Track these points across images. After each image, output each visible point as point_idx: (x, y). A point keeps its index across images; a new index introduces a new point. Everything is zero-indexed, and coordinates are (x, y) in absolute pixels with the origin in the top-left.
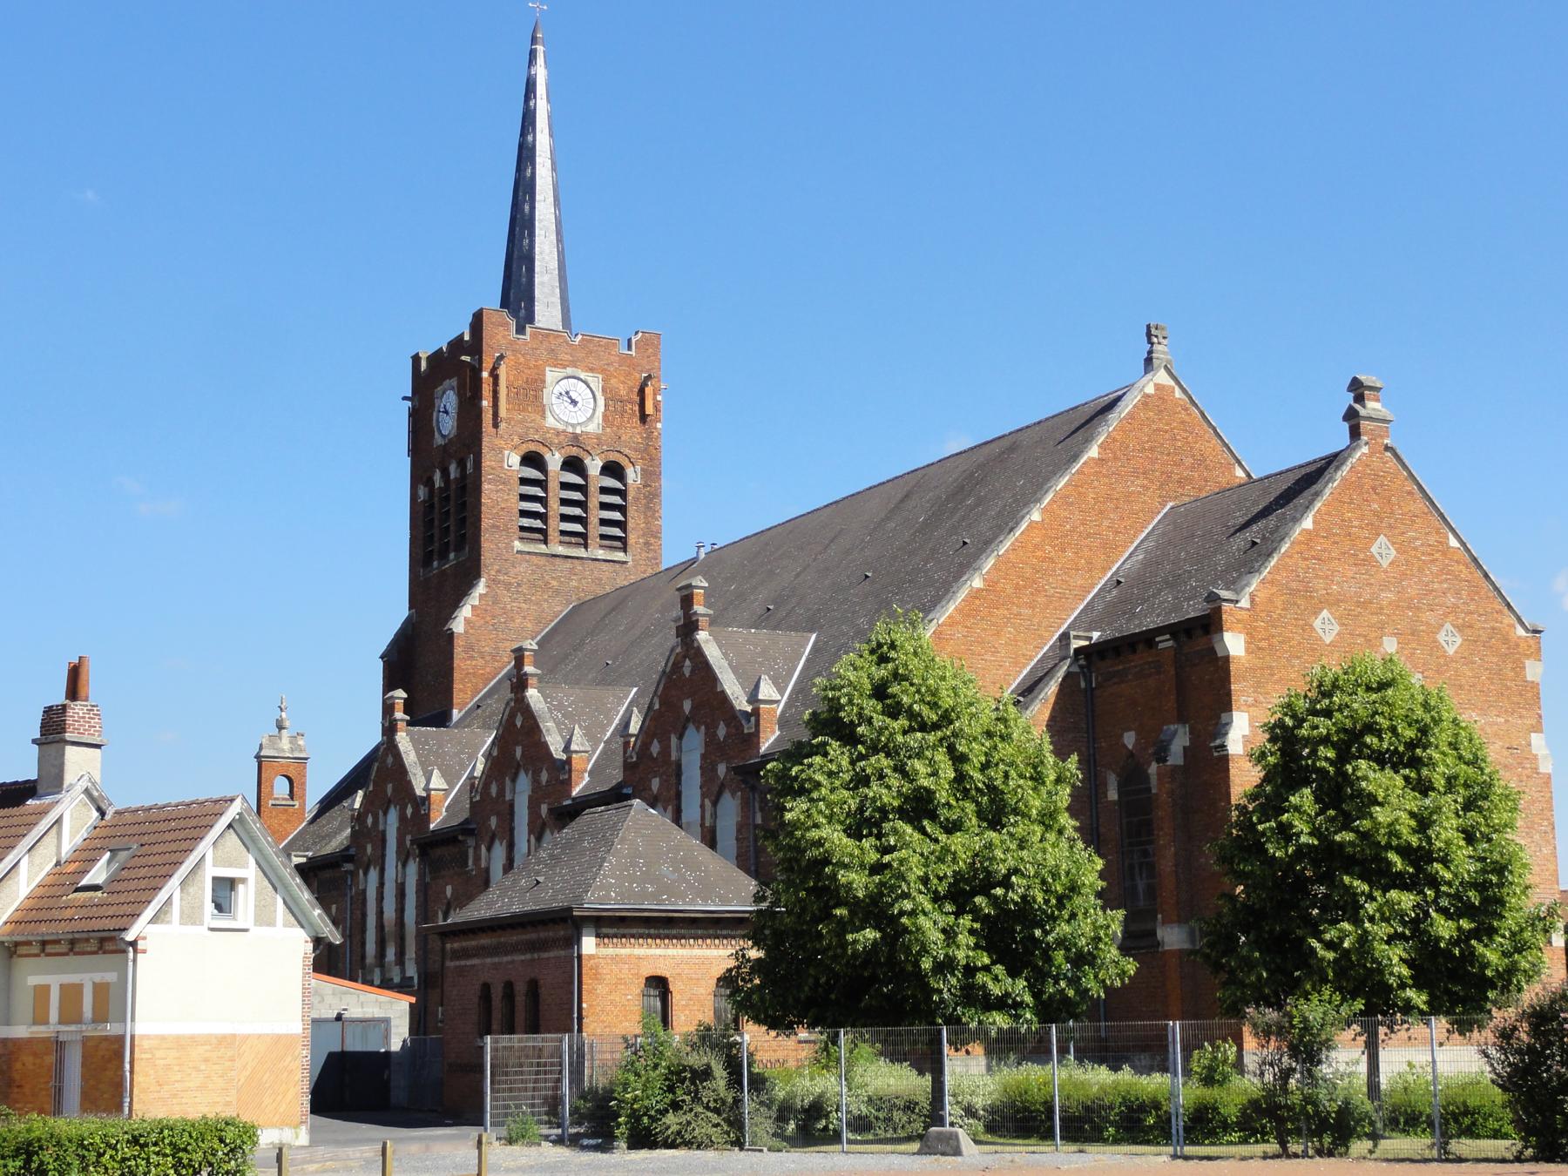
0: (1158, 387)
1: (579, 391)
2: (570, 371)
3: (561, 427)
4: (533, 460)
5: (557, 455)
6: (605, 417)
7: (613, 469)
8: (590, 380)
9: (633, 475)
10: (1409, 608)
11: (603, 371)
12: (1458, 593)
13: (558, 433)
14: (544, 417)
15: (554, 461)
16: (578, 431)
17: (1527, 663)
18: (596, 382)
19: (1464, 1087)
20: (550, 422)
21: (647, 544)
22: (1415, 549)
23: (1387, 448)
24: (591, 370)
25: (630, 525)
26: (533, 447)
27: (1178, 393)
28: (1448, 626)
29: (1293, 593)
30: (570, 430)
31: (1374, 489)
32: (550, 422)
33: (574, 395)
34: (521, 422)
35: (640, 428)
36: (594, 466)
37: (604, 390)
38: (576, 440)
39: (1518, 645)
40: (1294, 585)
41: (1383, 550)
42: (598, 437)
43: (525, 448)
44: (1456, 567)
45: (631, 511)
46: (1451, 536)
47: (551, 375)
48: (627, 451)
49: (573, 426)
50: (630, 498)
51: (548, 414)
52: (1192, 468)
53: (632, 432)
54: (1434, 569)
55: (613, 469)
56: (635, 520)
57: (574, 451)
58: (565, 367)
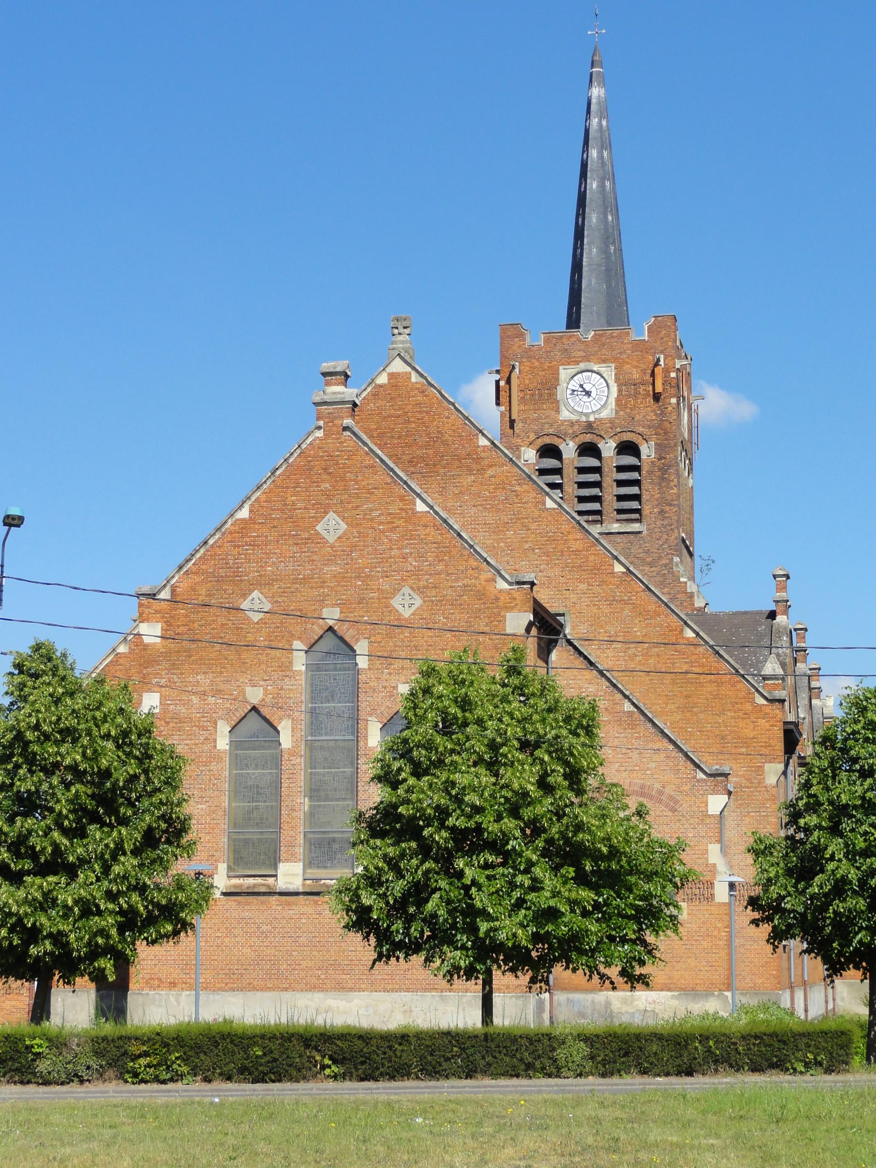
0: (392, 376)
1: (593, 382)
2: (582, 366)
3: (574, 417)
4: (550, 451)
5: (571, 444)
6: (618, 400)
7: (628, 448)
8: (603, 370)
9: (647, 451)
10: (358, 577)
11: (615, 360)
12: (421, 556)
13: (572, 424)
14: (558, 411)
15: (569, 449)
16: (592, 419)
17: (509, 615)
18: (609, 371)
19: (405, 1027)
20: (565, 414)
21: (662, 512)
22: (372, 520)
23: (346, 429)
24: (604, 361)
25: (644, 497)
26: (547, 440)
27: (414, 377)
28: (406, 590)
29: (220, 580)
30: (584, 419)
31: (325, 469)
32: (565, 414)
33: (587, 387)
34: (536, 420)
35: (655, 406)
36: (608, 448)
37: (617, 380)
38: (589, 427)
39: (497, 599)
40: (222, 572)
41: (332, 527)
42: (611, 421)
43: (540, 442)
44: (422, 532)
45: (645, 484)
46: (418, 501)
47: (564, 373)
48: (640, 429)
49: (587, 415)
50: (644, 472)
51: (562, 408)
52: (427, 446)
53: (646, 411)
54: (394, 537)
55: (628, 448)
56: (649, 491)
57: (588, 438)
58: (577, 363)
